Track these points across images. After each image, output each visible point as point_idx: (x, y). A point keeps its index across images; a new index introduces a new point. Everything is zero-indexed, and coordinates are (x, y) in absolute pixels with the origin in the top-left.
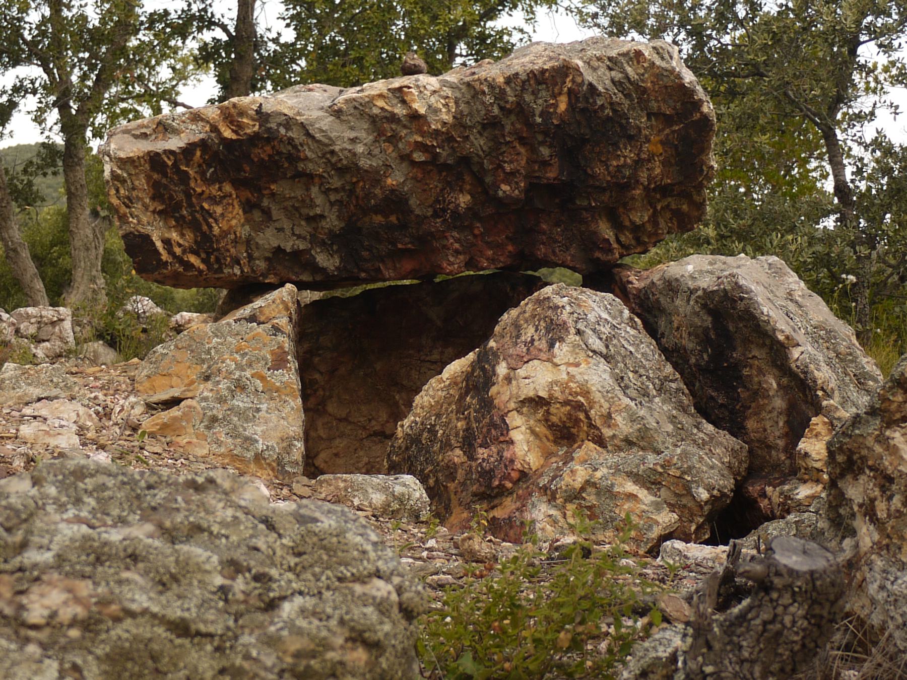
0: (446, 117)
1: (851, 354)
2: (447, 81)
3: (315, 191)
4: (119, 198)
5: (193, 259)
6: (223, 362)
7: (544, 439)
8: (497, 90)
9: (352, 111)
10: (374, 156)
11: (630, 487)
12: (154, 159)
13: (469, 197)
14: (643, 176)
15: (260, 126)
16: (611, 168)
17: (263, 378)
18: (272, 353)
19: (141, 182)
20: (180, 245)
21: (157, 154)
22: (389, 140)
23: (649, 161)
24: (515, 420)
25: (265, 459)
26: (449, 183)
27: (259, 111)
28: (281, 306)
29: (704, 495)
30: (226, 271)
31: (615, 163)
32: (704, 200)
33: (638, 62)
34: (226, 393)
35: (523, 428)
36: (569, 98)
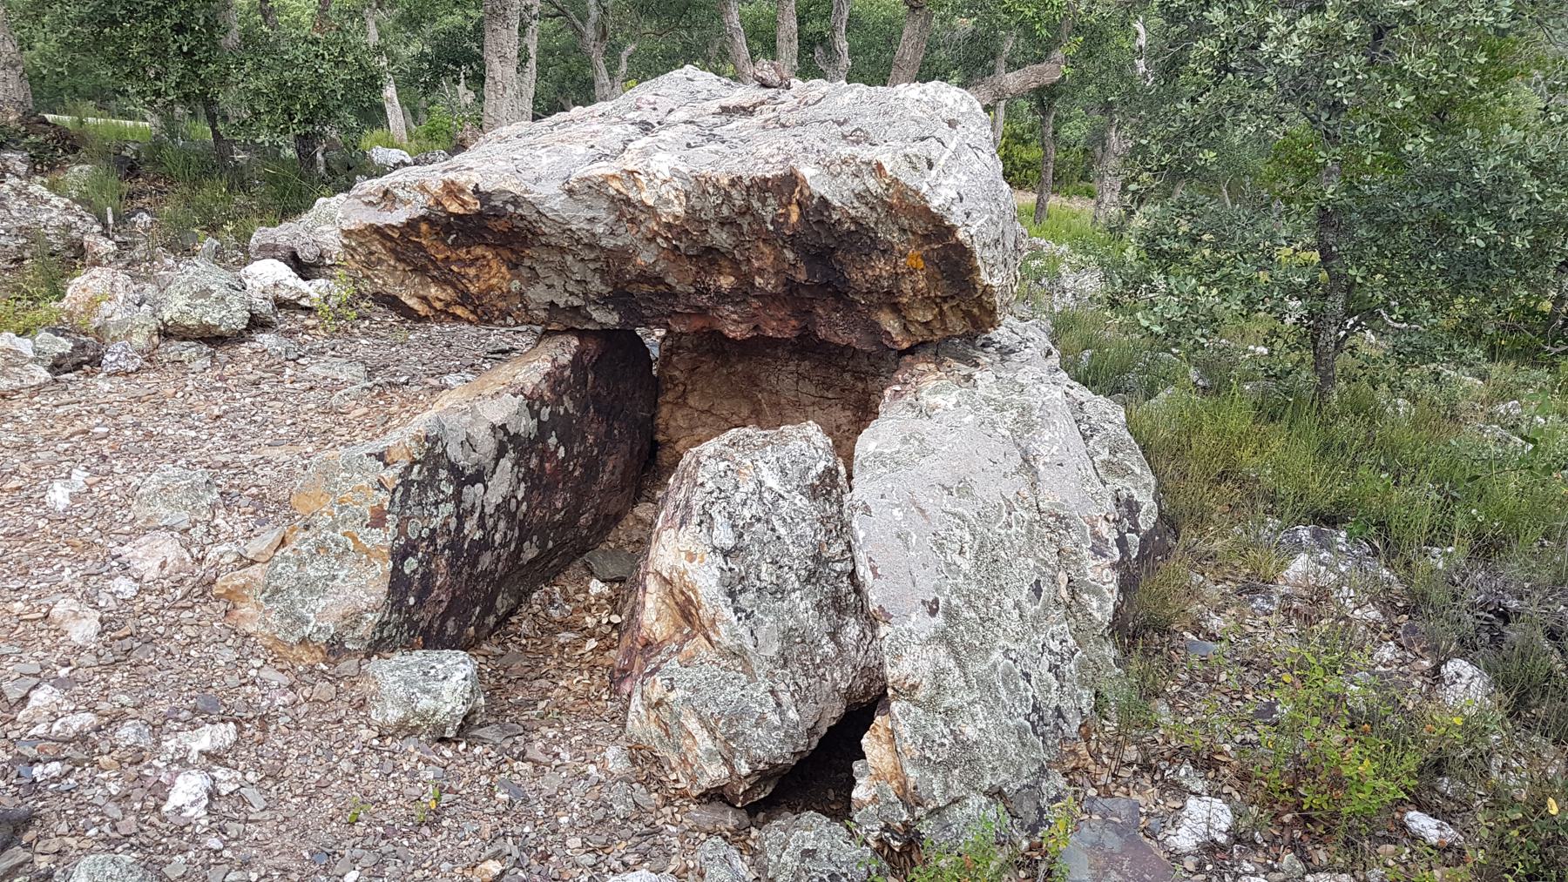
3: (569, 258)
5: (459, 311)
11: (692, 724)
14: (907, 287)
17: (354, 539)
18: (373, 510)
19: (376, 246)
22: (632, 221)
24: (652, 584)
27: (476, 191)
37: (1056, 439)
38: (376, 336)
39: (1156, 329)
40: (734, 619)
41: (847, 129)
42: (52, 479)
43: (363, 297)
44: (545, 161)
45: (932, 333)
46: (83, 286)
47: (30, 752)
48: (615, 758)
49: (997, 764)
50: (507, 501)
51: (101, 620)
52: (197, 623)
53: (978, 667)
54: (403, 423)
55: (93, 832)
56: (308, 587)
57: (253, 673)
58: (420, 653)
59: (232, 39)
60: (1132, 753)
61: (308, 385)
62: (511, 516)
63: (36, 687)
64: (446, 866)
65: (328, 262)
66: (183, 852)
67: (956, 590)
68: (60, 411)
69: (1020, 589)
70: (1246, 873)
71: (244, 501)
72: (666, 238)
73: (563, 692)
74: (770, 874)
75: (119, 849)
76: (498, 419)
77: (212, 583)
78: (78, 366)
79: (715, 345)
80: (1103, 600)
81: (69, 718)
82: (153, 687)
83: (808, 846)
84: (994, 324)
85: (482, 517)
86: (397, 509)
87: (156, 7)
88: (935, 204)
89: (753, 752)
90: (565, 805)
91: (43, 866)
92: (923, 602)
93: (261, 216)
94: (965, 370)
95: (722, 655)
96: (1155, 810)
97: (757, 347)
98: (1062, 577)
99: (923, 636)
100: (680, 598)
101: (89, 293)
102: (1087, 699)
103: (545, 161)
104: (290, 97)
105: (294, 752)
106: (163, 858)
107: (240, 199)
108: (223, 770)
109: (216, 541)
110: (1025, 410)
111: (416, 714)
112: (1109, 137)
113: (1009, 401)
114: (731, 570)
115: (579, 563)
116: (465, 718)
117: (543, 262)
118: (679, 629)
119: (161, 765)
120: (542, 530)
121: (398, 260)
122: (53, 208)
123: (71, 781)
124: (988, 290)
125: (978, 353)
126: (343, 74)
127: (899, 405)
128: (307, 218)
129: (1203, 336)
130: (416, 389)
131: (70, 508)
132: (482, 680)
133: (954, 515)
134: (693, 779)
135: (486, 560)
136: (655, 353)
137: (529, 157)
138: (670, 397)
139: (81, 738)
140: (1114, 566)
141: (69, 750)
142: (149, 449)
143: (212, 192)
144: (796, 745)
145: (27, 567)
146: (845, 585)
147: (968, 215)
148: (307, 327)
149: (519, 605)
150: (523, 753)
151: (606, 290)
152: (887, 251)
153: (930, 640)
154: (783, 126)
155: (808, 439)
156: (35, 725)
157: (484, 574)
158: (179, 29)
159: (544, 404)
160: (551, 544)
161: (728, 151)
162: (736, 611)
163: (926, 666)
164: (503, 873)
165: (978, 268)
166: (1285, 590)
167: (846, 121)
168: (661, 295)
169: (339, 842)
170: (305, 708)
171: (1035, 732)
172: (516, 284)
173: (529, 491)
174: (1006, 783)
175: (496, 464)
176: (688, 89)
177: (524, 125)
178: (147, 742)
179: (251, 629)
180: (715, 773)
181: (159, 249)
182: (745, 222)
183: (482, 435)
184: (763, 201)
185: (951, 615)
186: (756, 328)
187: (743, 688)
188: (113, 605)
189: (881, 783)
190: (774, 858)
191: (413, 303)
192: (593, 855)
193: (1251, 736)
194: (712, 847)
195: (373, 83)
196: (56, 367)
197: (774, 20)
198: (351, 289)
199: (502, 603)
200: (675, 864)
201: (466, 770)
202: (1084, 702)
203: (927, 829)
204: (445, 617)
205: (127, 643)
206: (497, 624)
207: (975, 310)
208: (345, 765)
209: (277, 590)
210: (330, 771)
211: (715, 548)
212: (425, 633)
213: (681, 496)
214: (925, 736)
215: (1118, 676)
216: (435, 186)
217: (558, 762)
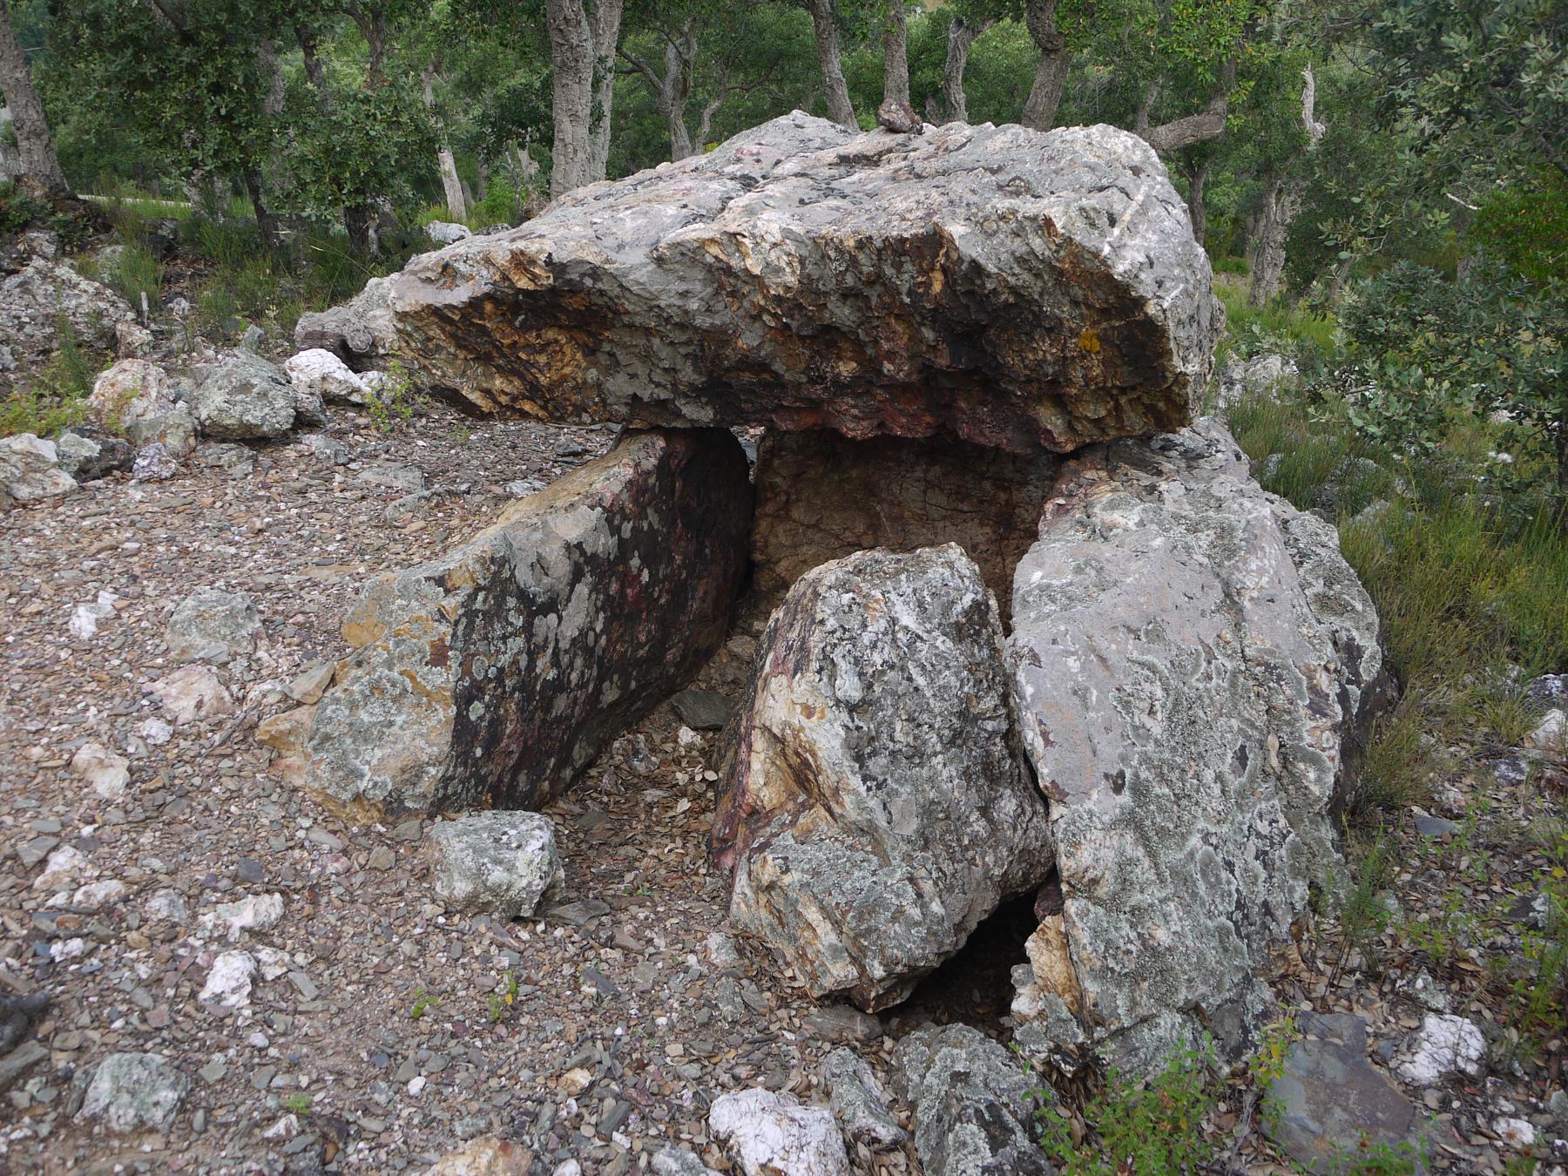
0: (791, 280)
1: (1290, 713)
3: (656, 341)
8: (847, 256)
11: (813, 914)
14: (1077, 374)
15: (555, 279)
17: (413, 679)
18: (433, 645)
19: (435, 332)
22: (733, 294)
24: (759, 741)
26: (818, 352)
34: (358, 697)
35: (762, 756)
37: (1264, 569)
38: (434, 437)
39: (1372, 429)
40: (863, 789)
41: (1002, 178)
42: (76, 602)
43: (419, 391)
44: (629, 224)
45: (1103, 431)
46: (115, 378)
47: (48, 926)
48: (718, 947)
49: (1194, 974)
50: (583, 633)
51: (130, 769)
52: (238, 774)
53: (1172, 856)
54: (464, 541)
55: (118, 1024)
56: (362, 734)
57: (301, 834)
58: (489, 813)
59: (275, 103)
60: (1355, 959)
61: (359, 494)
62: (589, 652)
63: (55, 848)
64: (525, 1074)
65: (381, 351)
66: (223, 1049)
67: (1146, 759)
68: (86, 523)
69: (1222, 757)
70: (1503, 1114)
71: (289, 630)
72: (774, 316)
73: (653, 862)
74: (910, 1097)
75: (149, 1045)
76: (573, 535)
77: (253, 727)
78: (106, 472)
79: (827, 445)
80: (1322, 770)
81: (94, 887)
82: (188, 849)
83: (960, 1068)
84: (1184, 421)
85: (556, 654)
86: (460, 645)
87: (190, 64)
88: (1120, 268)
89: (888, 952)
90: (662, 1003)
91: (62, 1065)
92: (1106, 776)
93: (308, 300)
94: (1147, 479)
95: (847, 831)
96: (1384, 1030)
97: (882, 448)
98: (1273, 741)
99: (1106, 818)
100: (795, 761)
101: (118, 388)
102: (1301, 891)
103: (629, 224)
104: (339, 165)
105: (349, 930)
106: (200, 1056)
107: (286, 282)
108: (269, 950)
109: (258, 679)
110: (1225, 531)
111: (487, 889)
112: (1268, 205)
113: (1204, 519)
114: (858, 728)
115: (665, 706)
116: (543, 894)
117: (625, 346)
118: (792, 796)
119: (198, 943)
120: (623, 667)
121: (459, 346)
122: (81, 295)
123: (95, 961)
124: (1181, 380)
125: (1159, 458)
126: (398, 137)
127: (1065, 523)
128: (358, 302)
129: (1429, 439)
130: (479, 498)
131: (96, 636)
132: (559, 842)
133: (1142, 664)
134: (814, 977)
135: (561, 704)
136: (752, 454)
137: (609, 223)
139: (107, 910)
140: (1335, 728)
141: (92, 925)
142: (186, 569)
143: (255, 274)
144: (941, 944)
145: (48, 705)
146: (998, 748)
147: (1160, 284)
148: (358, 427)
149: (598, 754)
150: (611, 938)
151: (699, 380)
152: (1055, 329)
153: (1114, 824)
154: (919, 176)
155: (950, 565)
156: (53, 894)
157: (559, 720)
158: (216, 89)
159: (625, 518)
160: (633, 684)
161: (851, 207)
162: (865, 780)
163: (1109, 856)
164: (592, 1084)
165: (1170, 352)
166: (1535, 754)
167: (1000, 169)
168: (765, 385)
169: (401, 1041)
170: (358, 879)
171: (1238, 933)
172: (593, 374)
173: (608, 623)
174: (1204, 997)
175: (572, 590)
176: (793, 140)
177: (602, 186)
178: (180, 915)
179: (298, 782)
180: (840, 972)
181: (199, 339)
182: (873, 295)
183: (554, 554)
184: (898, 267)
185: (1140, 791)
186: (881, 425)
187: (874, 873)
188: (143, 751)
189: (1051, 996)
190: (915, 1078)
191: (475, 397)
192: (696, 1066)
193: (1502, 939)
194: (838, 1059)
195: (429, 146)
196: (84, 472)
197: (882, 70)
198: (406, 382)
199: (579, 753)
200: (795, 1079)
201: (545, 956)
202: (1297, 896)
203: (1108, 1053)
204: (516, 770)
205: (159, 797)
206: (575, 778)
207: (1161, 405)
208: (407, 948)
209: (327, 738)
210: (391, 953)
211: (838, 702)
212: (495, 790)
213: (794, 635)
214: (1108, 943)
215: (1338, 862)
216: (502, 258)
217: (651, 950)
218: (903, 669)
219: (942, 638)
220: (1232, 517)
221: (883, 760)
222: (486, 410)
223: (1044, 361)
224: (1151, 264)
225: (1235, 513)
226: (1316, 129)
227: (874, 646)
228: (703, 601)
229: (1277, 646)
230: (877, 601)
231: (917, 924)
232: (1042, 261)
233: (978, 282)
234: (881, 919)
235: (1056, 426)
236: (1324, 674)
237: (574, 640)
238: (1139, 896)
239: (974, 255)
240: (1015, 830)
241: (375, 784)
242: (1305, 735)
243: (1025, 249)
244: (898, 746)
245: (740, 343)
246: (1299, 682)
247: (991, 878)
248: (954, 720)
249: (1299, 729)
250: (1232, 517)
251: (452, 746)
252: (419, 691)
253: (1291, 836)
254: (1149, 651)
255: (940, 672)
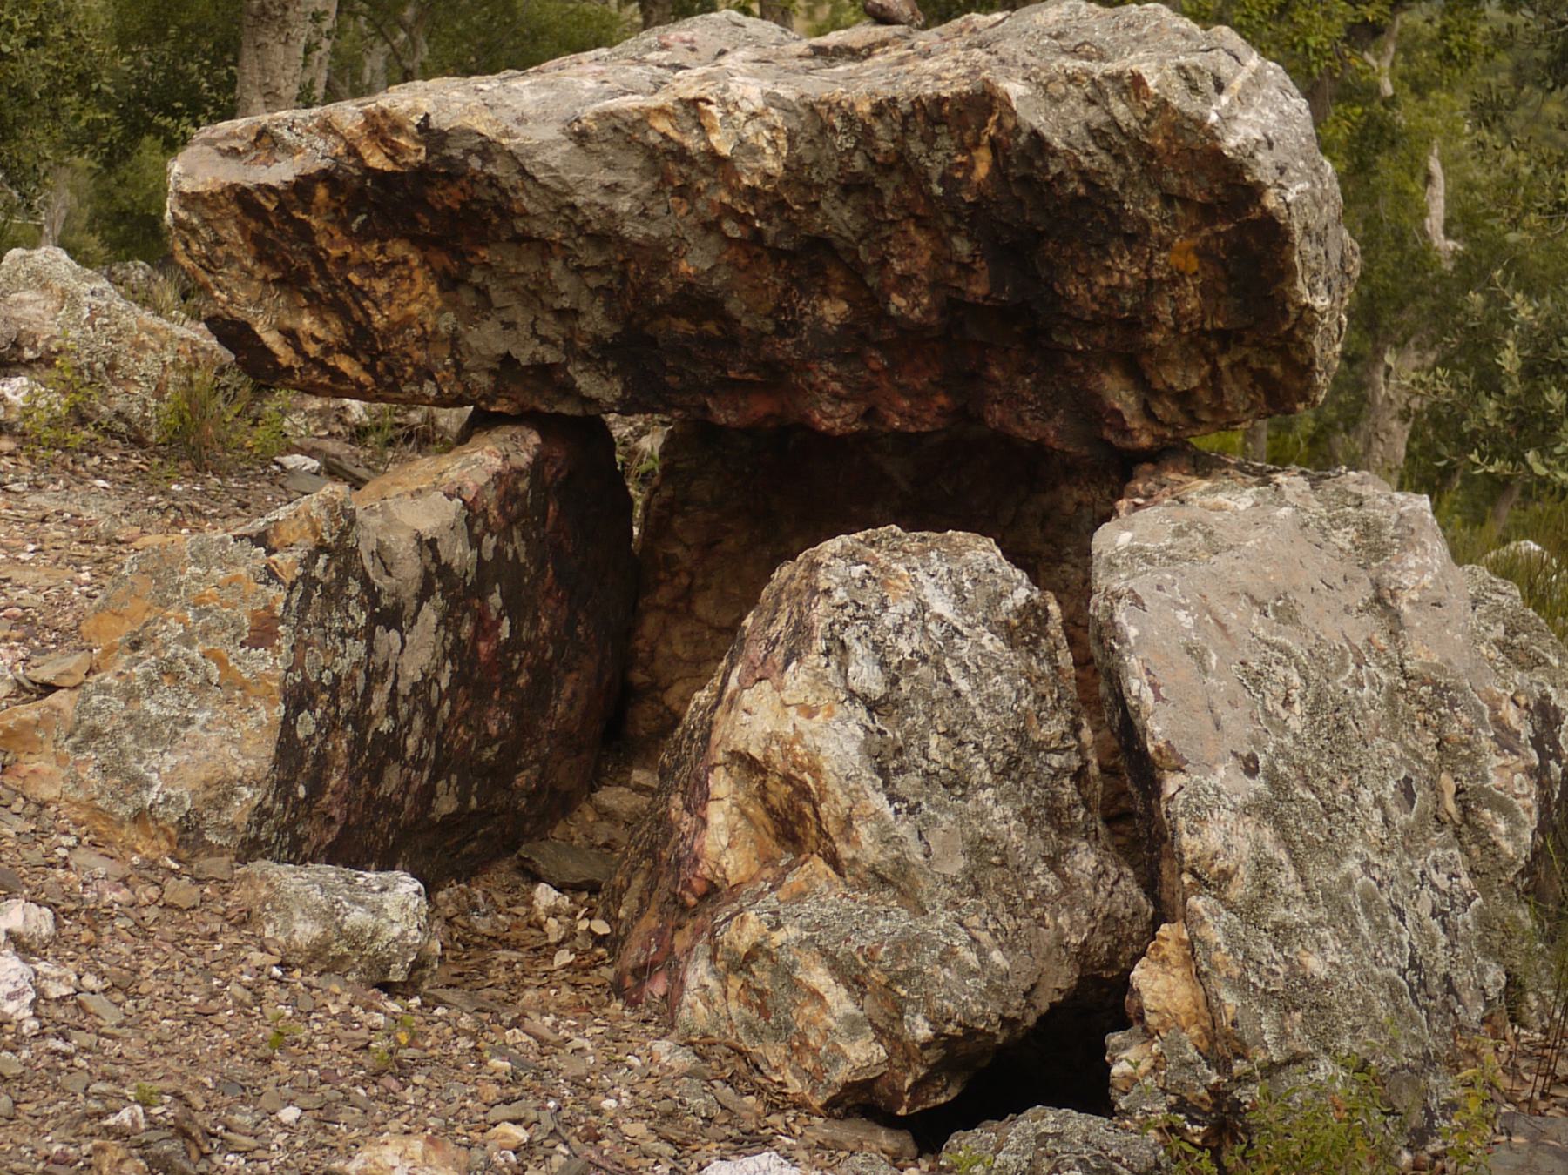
0: (773, 165)
1: (1468, 745)
2: (777, 97)
3: (556, 266)
4: (191, 258)
5: (345, 364)
6: (164, 622)
7: (762, 830)
9: (610, 135)
10: (654, 219)
11: (819, 977)
12: (242, 197)
13: (844, 306)
14: (1164, 309)
15: (428, 157)
16: (1096, 290)
17: (221, 662)
18: (254, 616)
19: (231, 232)
20: (317, 341)
21: (245, 190)
22: (681, 192)
23: (1174, 282)
24: (721, 784)
25: (156, 820)
26: (795, 281)
27: (424, 127)
28: (307, 526)
29: (923, 1031)
30: (406, 389)
31: (1102, 281)
32: (1312, 362)
33: (1137, 96)
35: (727, 803)
36: (995, 154)
40: (889, 811)
44: (527, 96)
49: (1360, 1020)
56: (149, 732)
57: (62, 852)
65: (28, 354)
67: (1281, 752)
72: (743, 220)
88: (1230, 143)
89: (936, 1004)
92: (1235, 754)
98: (1448, 783)
102: (1494, 976)
111: (342, 934)
118: (768, 861)
121: (260, 258)
133: (1273, 646)
138: (663, 596)
144: (1007, 1006)
147: (1282, 171)
152: (1135, 238)
159: (487, 527)
172: (448, 321)
179: (47, 792)
180: (864, 1053)
184: (929, 140)
185: (1274, 780)
191: (272, 339)
202: (1489, 979)
207: (1276, 369)
209: (94, 733)
218: (938, 666)
219: (989, 636)
220: (1378, 512)
221: (914, 779)
222: (284, 362)
223: (1121, 287)
224: (1270, 145)
225: (1382, 508)
226: (1444, 245)
227: (899, 631)
228: (571, 706)
229: (1449, 662)
230: (899, 577)
231: (973, 973)
232: (1126, 136)
233: (1039, 163)
234: (926, 961)
235: (1126, 405)
236: (1512, 707)
237: (415, 685)
238: (1283, 911)
239: (1036, 124)
240: (1096, 891)
241: (168, 798)
242: (1491, 774)
243: (1103, 118)
244: (933, 767)
245: (684, 266)
246: (1480, 710)
247: (1065, 947)
248: (1010, 741)
249: (1482, 767)
250: (1378, 512)
251: (275, 762)
252: (231, 682)
253: (1479, 901)
254: (1279, 633)
255: (988, 676)
